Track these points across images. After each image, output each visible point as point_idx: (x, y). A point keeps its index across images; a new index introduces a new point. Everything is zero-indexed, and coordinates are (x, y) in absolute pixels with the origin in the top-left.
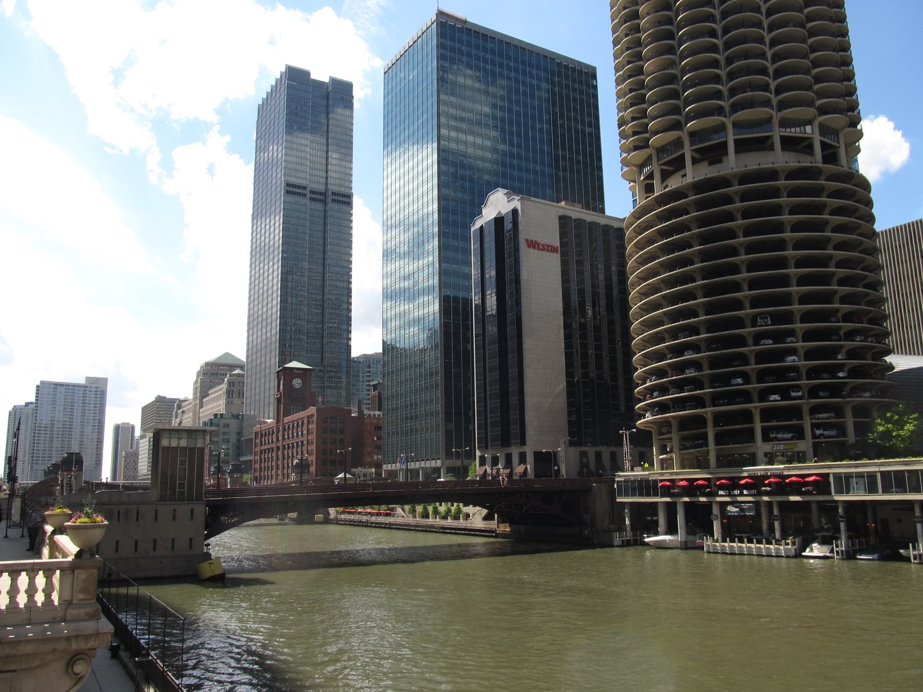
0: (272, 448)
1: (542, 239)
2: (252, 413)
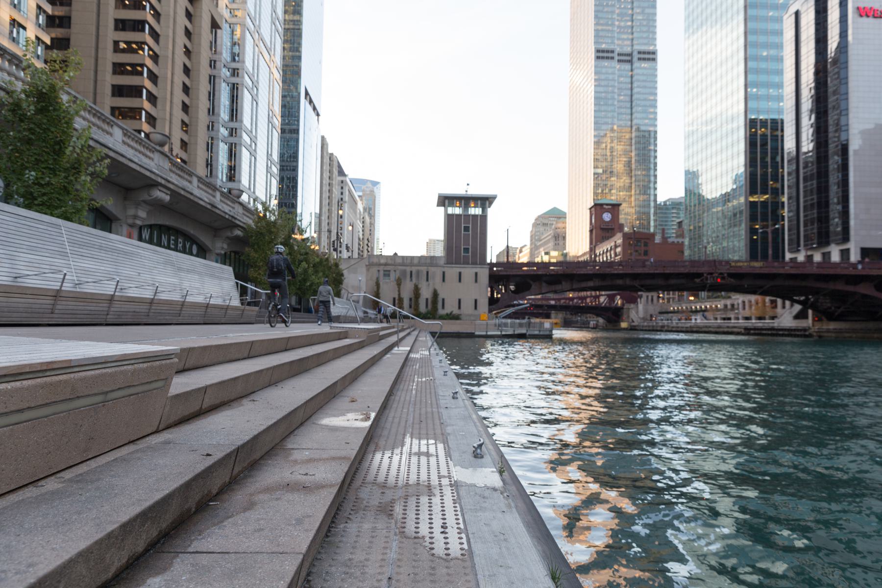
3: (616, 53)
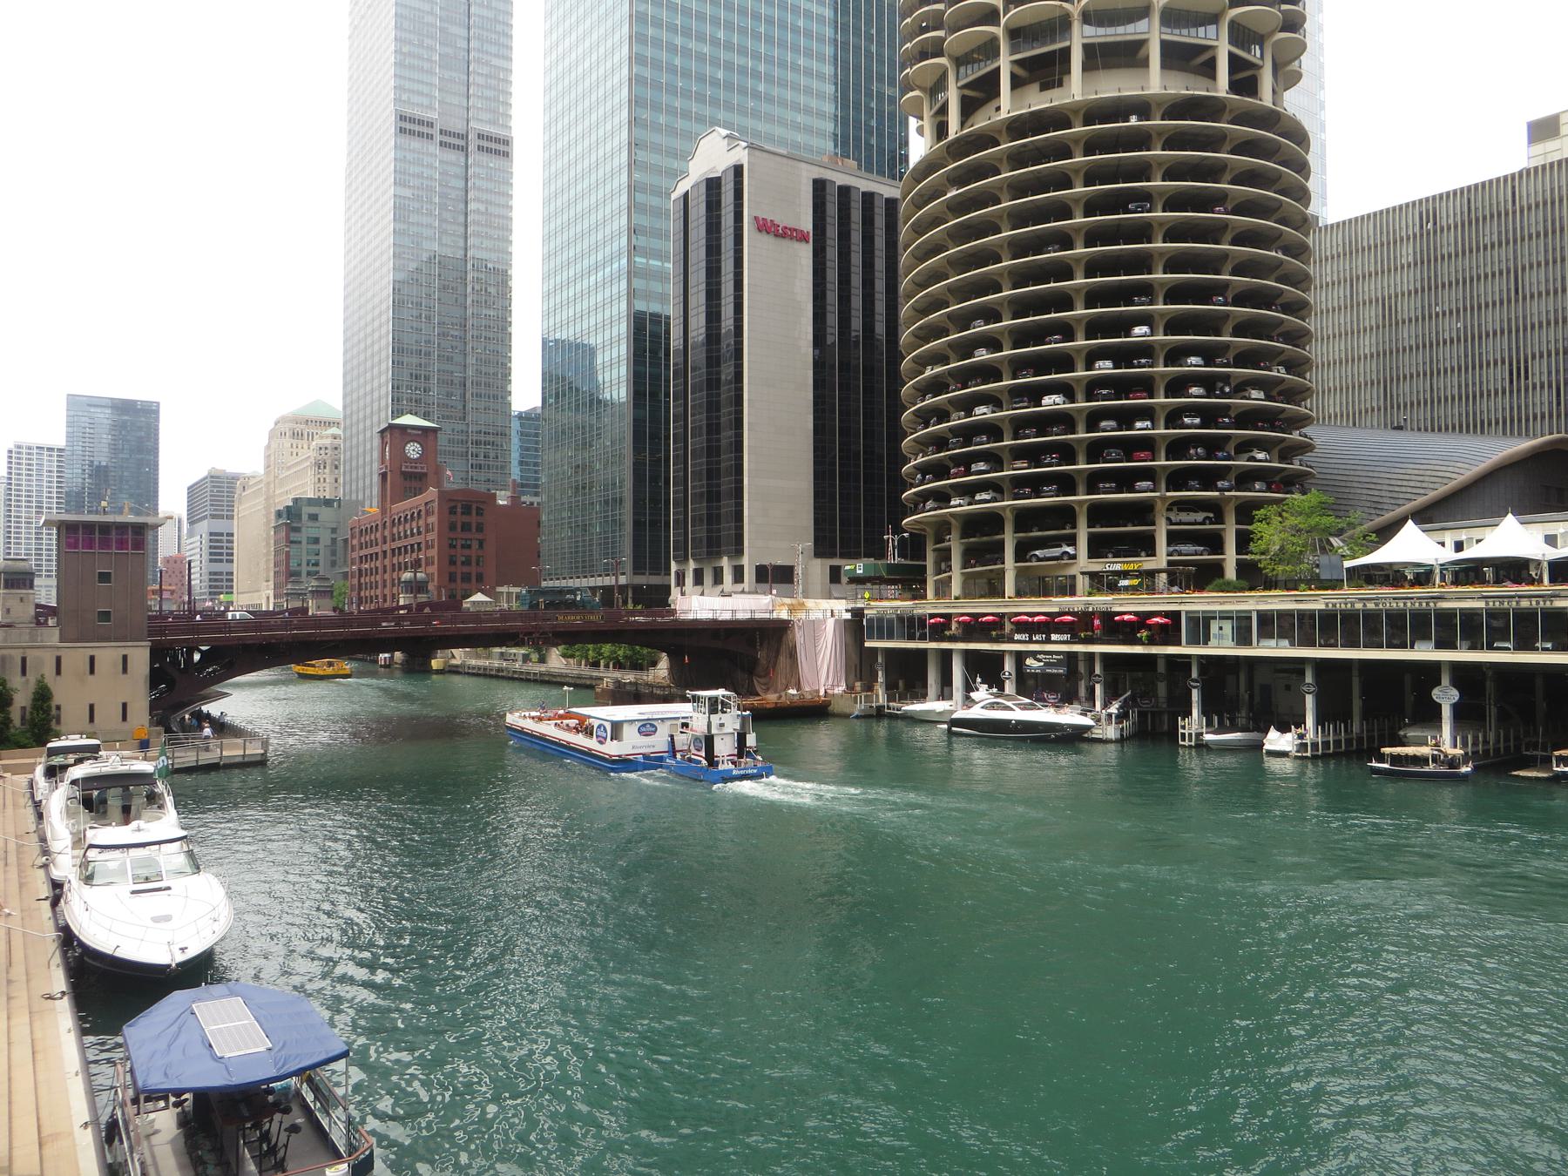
0: (419, 544)
1: (782, 219)
2: (354, 497)
3: (438, 127)
